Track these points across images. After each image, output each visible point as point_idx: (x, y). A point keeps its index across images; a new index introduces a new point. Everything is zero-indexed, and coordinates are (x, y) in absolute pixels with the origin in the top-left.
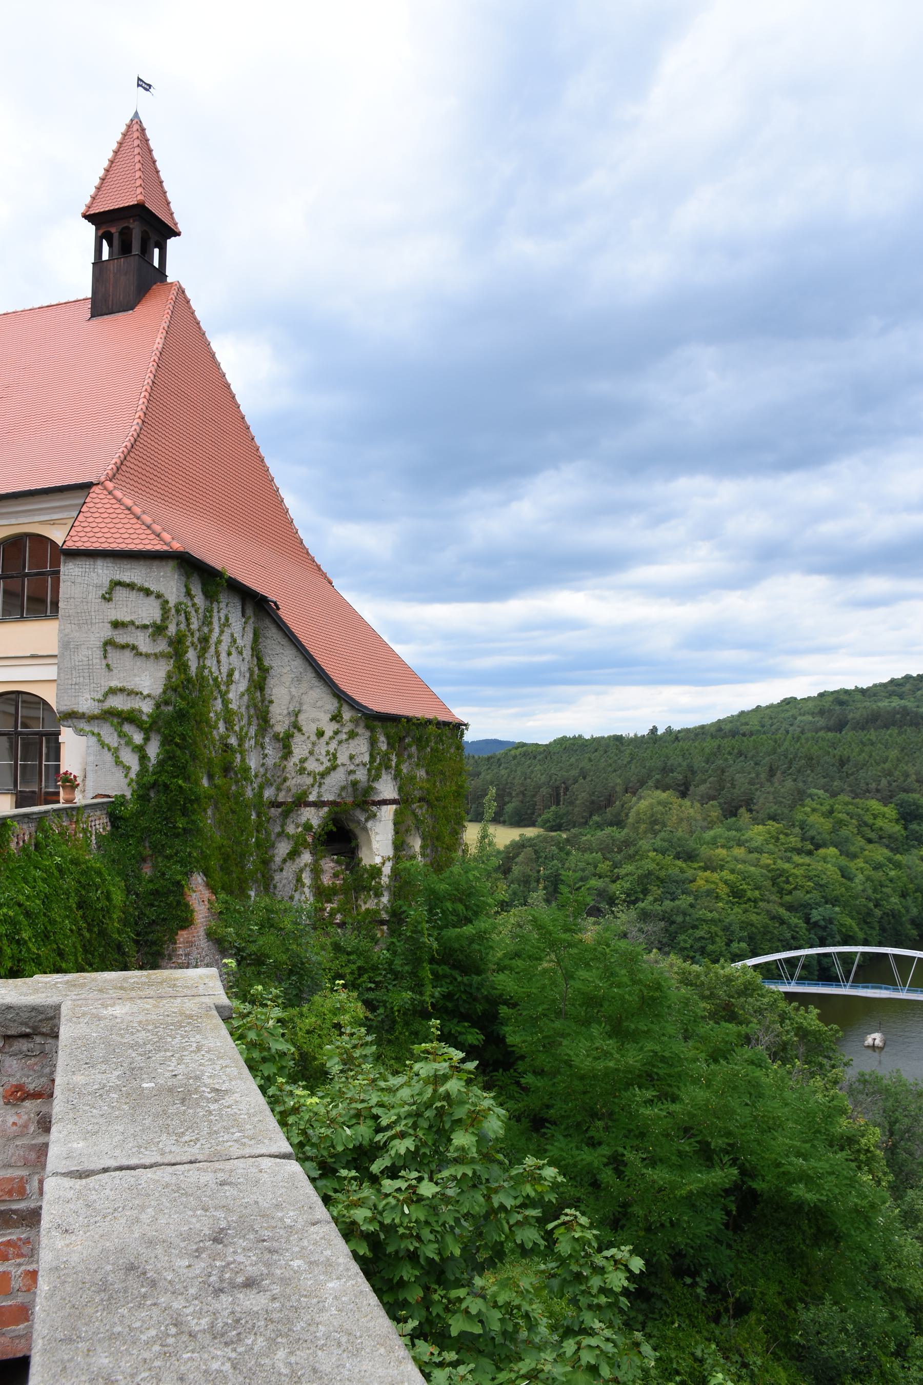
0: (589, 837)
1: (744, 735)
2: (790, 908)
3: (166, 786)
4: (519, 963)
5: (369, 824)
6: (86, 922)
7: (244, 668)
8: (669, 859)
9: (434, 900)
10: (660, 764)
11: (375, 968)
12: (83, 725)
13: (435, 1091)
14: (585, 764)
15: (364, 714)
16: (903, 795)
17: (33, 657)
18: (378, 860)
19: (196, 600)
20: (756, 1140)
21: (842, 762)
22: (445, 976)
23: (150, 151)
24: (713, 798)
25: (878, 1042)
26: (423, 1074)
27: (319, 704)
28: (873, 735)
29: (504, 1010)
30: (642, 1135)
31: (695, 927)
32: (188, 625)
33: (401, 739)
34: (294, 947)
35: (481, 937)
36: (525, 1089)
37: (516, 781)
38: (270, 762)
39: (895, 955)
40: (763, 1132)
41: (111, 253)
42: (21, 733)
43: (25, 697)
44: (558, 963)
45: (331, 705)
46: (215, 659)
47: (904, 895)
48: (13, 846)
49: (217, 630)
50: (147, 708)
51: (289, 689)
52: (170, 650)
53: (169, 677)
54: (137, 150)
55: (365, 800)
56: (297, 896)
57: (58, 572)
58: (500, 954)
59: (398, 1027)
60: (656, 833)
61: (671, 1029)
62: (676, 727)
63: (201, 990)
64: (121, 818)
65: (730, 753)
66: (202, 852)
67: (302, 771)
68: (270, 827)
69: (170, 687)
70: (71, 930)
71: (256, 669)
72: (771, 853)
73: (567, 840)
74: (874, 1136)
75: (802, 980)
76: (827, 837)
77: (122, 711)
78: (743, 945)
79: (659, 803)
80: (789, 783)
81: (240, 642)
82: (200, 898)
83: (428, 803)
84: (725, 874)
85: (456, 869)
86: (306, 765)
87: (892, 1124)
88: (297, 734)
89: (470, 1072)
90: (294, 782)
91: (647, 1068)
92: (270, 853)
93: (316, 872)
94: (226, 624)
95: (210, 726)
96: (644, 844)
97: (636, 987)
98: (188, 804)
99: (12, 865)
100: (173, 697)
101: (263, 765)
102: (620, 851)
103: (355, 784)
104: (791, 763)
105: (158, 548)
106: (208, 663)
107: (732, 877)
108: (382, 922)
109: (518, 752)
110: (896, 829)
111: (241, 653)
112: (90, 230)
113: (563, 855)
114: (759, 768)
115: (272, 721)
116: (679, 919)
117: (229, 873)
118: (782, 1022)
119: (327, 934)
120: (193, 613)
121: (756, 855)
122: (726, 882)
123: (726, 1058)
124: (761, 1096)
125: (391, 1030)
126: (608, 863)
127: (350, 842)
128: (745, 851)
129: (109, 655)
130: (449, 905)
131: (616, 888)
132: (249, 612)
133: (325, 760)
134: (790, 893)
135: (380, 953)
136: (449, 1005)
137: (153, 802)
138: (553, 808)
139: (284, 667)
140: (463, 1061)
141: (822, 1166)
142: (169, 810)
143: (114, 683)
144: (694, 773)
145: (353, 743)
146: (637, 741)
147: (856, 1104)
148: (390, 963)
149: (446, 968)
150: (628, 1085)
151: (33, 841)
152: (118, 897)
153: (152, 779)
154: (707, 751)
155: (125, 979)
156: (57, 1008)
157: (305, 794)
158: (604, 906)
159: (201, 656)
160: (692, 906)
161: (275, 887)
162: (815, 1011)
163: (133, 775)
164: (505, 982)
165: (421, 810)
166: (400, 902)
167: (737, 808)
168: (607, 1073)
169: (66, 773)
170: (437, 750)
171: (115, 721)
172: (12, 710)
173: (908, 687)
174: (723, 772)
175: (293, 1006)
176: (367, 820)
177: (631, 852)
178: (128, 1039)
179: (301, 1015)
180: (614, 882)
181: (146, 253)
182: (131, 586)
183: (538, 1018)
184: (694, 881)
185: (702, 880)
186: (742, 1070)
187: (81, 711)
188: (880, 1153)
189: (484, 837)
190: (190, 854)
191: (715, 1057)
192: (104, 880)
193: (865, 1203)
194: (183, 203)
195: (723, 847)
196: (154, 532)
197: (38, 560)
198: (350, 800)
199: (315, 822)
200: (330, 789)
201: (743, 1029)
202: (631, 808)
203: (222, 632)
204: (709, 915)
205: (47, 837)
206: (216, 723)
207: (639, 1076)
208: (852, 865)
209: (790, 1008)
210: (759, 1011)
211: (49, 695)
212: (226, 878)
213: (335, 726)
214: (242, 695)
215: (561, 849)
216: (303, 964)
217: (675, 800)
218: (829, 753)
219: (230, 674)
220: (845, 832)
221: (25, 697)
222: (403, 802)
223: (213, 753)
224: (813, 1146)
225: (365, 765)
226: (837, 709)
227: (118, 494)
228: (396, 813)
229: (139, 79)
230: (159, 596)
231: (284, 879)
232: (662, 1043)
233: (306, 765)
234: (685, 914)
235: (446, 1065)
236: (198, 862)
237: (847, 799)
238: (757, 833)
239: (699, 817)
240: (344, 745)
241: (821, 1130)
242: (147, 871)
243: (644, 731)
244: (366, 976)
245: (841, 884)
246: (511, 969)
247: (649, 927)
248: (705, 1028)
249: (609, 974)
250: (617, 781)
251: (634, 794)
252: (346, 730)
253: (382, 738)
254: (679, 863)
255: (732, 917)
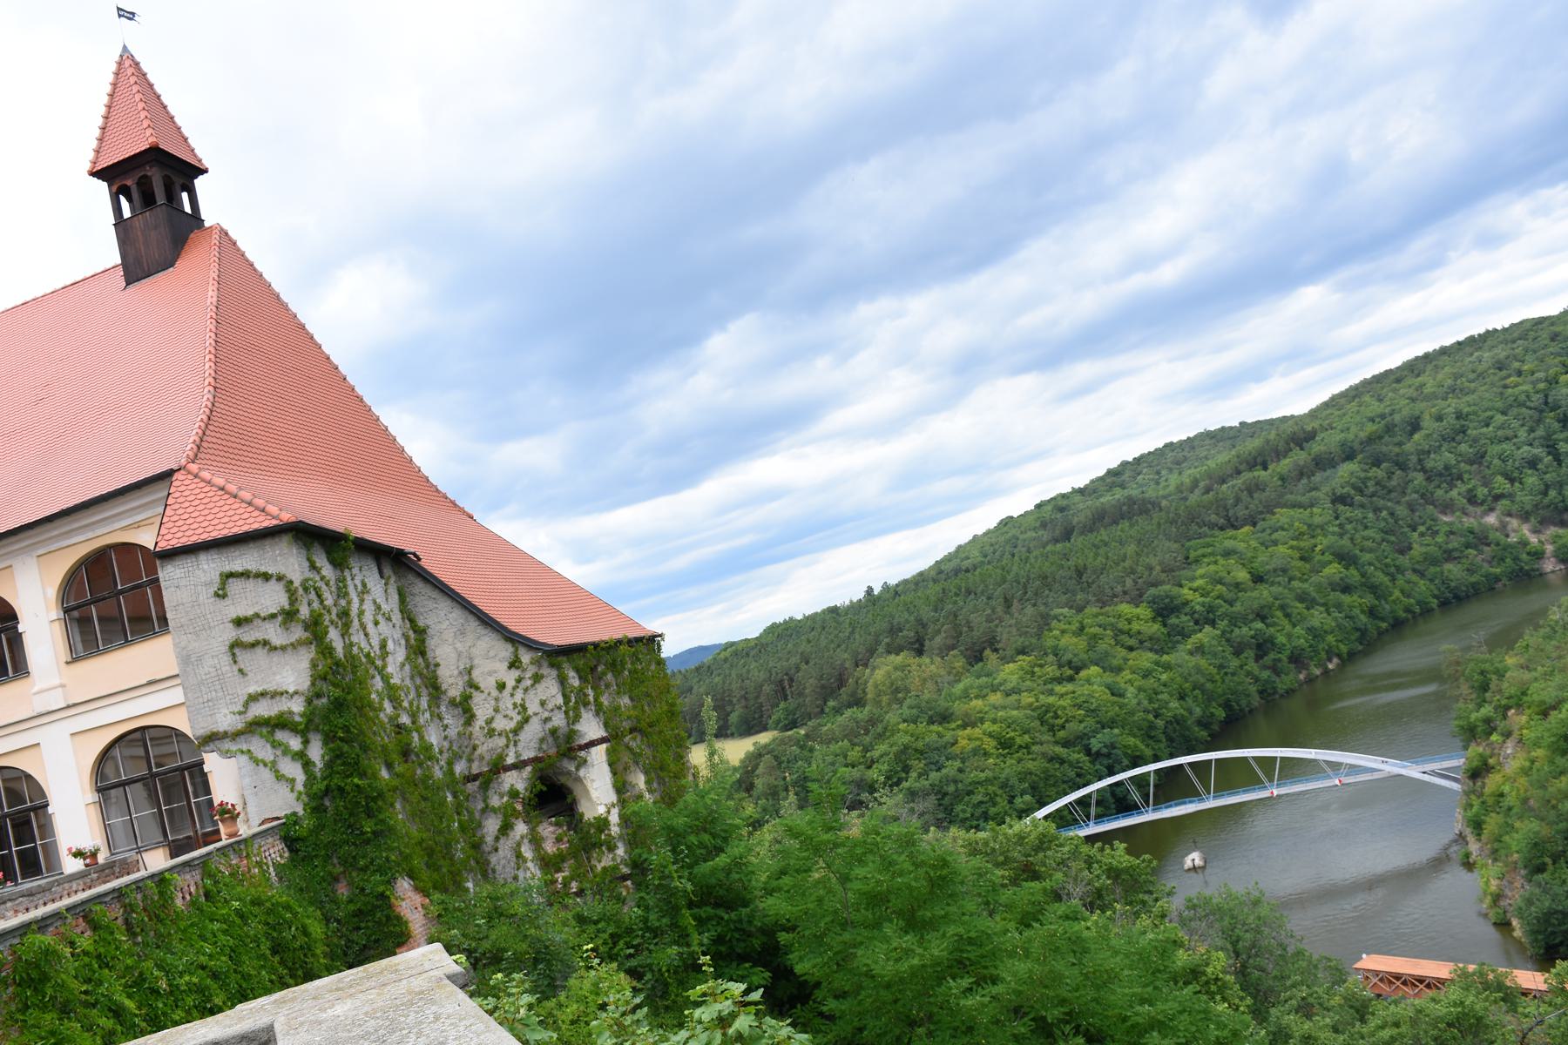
0: (833, 725)
1: (967, 571)
2: (1066, 744)
3: (341, 790)
4: (786, 880)
5: (582, 773)
6: (286, 967)
7: (397, 634)
8: (922, 727)
9: (675, 838)
10: (885, 625)
11: (629, 931)
12: (227, 745)
13: (724, 1034)
14: (804, 647)
15: (545, 652)
16: (1152, 591)
17: (150, 683)
18: (601, 810)
19: (324, 572)
20: (1095, 1000)
21: (1080, 573)
22: (709, 919)
23: (151, 86)
24: (953, 647)
25: (1198, 862)
26: (706, 1018)
27: (492, 653)
28: (1104, 534)
29: (783, 937)
30: (970, 1029)
31: (970, 793)
32: (322, 602)
33: (593, 669)
34: (533, 931)
35: (738, 864)
36: (830, 1018)
37: (734, 686)
38: (452, 733)
39: (1190, 764)
40: (1098, 988)
41: (132, 209)
42: (157, 774)
43: (153, 732)
44: (829, 866)
45: (505, 651)
46: (361, 634)
47: (1182, 698)
48: (179, 902)
49: (356, 600)
50: (297, 707)
51: (456, 648)
52: (307, 635)
53: (314, 665)
54: (135, 88)
55: (569, 748)
56: (521, 874)
57: (157, 580)
58: (763, 878)
59: (673, 989)
60: (900, 702)
61: (971, 906)
62: (893, 582)
63: (427, 966)
64: (298, 839)
65: (957, 595)
66: (401, 853)
67: (491, 733)
68: (471, 805)
69: (318, 677)
70: (271, 981)
71: (411, 633)
72: (1030, 690)
73: (807, 735)
74: (1219, 963)
75: (1100, 818)
76: (1085, 656)
77: (270, 718)
78: (1027, 798)
79: (896, 668)
80: (1029, 610)
81: (385, 607)
82: (409, 903)
83: (640, 731)
84: (988, 726)
85: (690, 797)
86: (494, 725)
87: (1235, 943)
88: (475, 693)
89: (756, 1003)
90: (485, 748)
91: (956, 955)
92: (479, 834)
93: (536, 841)
94: (365, 590)
95: (375, 710)
96: (892, 717)
97: (921, 871)
98: (371, 803)
99: (182, 925)
100: (325, 687)
101: (446, 738)
102: (867, 732)
103: (554, 732)
104: (1025, 587)
105: (266, 524)
106: (355, 639)
107: (995, 728)
108: (624, 878)
109: (727, 654)
110: (1155, 628)
111: (389, 619)
112: (102, 187)
113: (806, 753)
114: (993, 603)
115: (444, 687)
116: (951, 788)
117: (438, 869)
118: (1089, 868)
119: (566, 907)
120: (324, 587)
121: (1014, 697)
122: (990, 735)
123: (1038, 920)
124: (1086, 951)
125: (665, 995)
126: (857, 748)
127: (565, 798)
128: (1001, 696)
129: (239, 659)
130: (693, 839)
131: (874, 774)
132: (388, 571)
133: (513, 714)
134: (1063, 727)
135: (631, 912)
136: (723, 949)
137: (331, 811)
138: (782, 705)
139: (441, 620)
140: (746, 992)
141: (1171, 1007)
142: (351, 815)
143: (253, 689)
144: (924, 626)
145: (540, 687)
146: (855, 607)
147: (1191, 932)
148: (645, 920)
149: (708, 909)
150: (940, 979)
151: (201, 892)
152: (317, 929)
153: (322, 786)
154: (933, 599)
155: (340, 981)
156: (270, 1029)
157: (501, 757)
158: (865, 796)
159: (345, 633)
160: (960, 770)
161: (494, 871)
162: (1121, 846)
163: (300, 787)
164: (774, 907)
165: (635, 742)
166: (637, 851)
167: (982, 651)
168: (914, 973)
169: (221, 804)
170: (636, 671)
171: (264, 731)
172: (141, 752)
173: (1126, 477)
174: (956, 616)
175: (548, 998)
176: (578, 769)
177: (880, 729)
178: (357, 1031)
179: (560, 1006)
180: (870, 767)
181: (172, 199)
182: (245, 575)
183: (824, 934)
184: (956, 742)
185: (965, 739)
186: (1058, 928)
187: (221, 730)
188: (1230, 978)
189: (712, 754)
190: (387, 859)
191: (1025, 922)
192: (295, 914)
193: (1226, 1033)
194: (202, 138)
195: (977, 697)
196: (257, 509)
197: (130, 572)
198: (552, 751)
199: (521, 786)
200: (529, 745)
201: (1047, 884)
202: (866, 682)
203: (362, 601)
204: (983, 776)
205: (216, 882)
206: (381, 703)
207: (950, 967)
208: (1118, 679)
209: (1094, 851)
210: (1062, 863)
211: (180, 722)
212: (435, 876)
213: (515, 674)
214: (403, 665)
215: (802, 748)
216: (547, 947)
217: (912, 661)
218: (1062, 567)
219: (383, 645)
220: (1102, 646)
221: (153, 732)
222: (612, 737)
223: (386, 739)
224: (1156, 988)
225: (559, 708)
226: (1059, 519)
227: (206, 475)
228: (608, 752)
229: (119, 9)
230: (280, 578)
231: (501, 860)
232: (963, 923)
233: (494, 725)
234: (956, 782)
235: (729, 1002)
236: (399, 865)
237: (1095, 610)
238: (1010, 672)
239: (943, 672)
240: (531, 692)
241: (1156, 967)
242: (343, 891)
243: (859, 594)
244: (621, 943)
245: (1114, 703)
246: (779, 889)
247: (920, 806)
248: (1007, 895)
249: (888, 864)
250: (844, 657)
251: (866, 665)
252: (528, 674)
253: (572, 674)
254: (935, 728)
255: (1007, 771)
